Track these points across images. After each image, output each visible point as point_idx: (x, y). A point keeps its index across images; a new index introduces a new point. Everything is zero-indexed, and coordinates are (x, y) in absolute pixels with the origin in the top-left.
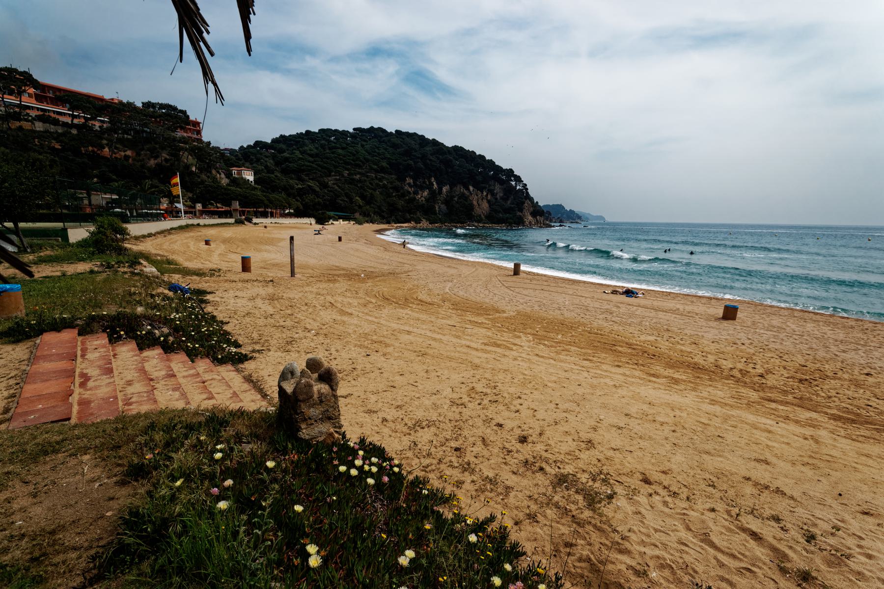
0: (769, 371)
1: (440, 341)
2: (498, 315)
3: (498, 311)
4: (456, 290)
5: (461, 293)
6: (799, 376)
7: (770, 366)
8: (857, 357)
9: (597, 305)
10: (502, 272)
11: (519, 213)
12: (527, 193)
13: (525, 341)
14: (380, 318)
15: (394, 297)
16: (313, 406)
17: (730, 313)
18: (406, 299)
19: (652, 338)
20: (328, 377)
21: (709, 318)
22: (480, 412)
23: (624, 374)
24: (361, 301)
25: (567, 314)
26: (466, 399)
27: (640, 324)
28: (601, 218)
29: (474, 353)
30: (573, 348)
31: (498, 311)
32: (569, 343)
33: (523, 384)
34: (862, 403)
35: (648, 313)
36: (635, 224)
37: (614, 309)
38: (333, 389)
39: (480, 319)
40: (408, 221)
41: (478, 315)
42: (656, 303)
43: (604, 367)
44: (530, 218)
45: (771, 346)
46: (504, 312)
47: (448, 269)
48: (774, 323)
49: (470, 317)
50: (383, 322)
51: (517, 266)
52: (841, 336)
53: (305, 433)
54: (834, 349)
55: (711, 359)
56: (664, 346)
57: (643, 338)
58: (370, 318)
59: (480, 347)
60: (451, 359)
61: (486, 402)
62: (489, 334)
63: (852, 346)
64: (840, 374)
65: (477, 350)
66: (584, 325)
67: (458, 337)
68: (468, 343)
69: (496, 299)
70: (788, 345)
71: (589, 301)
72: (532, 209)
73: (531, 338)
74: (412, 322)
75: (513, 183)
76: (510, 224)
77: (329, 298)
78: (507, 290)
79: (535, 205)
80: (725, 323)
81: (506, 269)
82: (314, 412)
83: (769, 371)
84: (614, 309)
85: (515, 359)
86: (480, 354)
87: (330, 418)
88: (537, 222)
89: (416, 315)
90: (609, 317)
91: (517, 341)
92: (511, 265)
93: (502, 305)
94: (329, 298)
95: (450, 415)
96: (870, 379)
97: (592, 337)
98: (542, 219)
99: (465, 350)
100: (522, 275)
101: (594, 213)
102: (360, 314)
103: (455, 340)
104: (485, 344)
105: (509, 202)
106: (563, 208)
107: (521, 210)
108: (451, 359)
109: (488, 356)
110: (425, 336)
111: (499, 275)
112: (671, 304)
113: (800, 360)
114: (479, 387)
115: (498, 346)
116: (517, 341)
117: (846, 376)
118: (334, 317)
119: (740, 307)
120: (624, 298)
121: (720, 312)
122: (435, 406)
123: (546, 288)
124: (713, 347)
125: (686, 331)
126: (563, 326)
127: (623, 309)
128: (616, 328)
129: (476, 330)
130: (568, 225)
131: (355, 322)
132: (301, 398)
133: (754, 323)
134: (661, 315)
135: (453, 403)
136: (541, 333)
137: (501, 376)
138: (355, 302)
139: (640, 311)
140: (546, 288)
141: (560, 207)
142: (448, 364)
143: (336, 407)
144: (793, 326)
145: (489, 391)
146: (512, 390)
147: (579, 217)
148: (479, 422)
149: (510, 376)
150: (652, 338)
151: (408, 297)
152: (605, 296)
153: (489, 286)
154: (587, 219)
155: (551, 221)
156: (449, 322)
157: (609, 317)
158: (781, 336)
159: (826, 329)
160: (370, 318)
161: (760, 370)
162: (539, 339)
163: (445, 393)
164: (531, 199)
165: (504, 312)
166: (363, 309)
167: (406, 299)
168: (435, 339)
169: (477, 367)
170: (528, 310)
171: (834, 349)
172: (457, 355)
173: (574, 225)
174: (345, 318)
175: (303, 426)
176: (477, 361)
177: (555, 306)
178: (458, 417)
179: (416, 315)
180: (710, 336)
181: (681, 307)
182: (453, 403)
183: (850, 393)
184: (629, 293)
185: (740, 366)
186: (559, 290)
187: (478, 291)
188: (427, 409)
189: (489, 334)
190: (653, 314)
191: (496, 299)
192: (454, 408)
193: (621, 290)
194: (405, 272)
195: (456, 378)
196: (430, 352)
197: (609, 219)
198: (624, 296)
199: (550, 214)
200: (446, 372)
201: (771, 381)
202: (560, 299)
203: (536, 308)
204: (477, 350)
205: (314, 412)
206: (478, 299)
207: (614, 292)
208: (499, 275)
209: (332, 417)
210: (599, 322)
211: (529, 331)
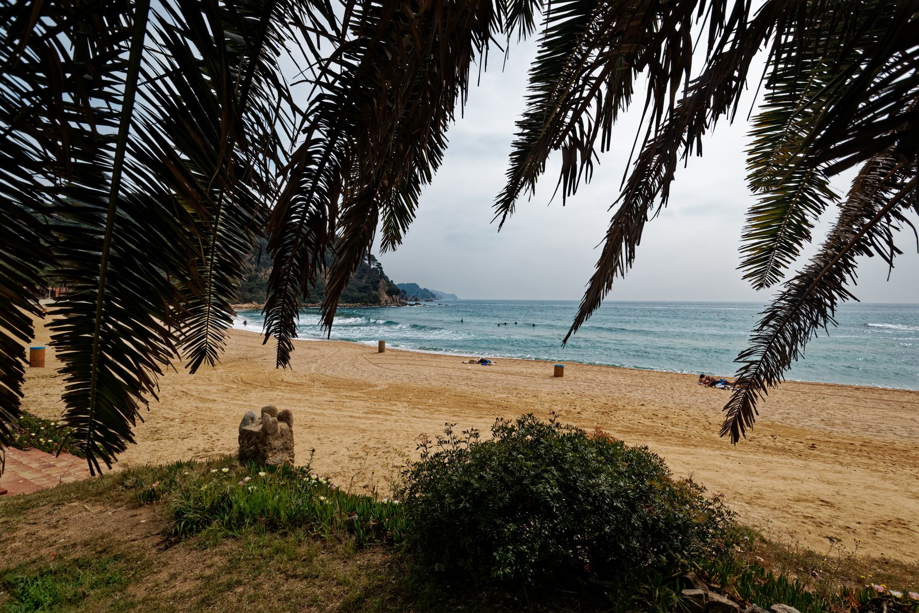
0: (584, 410)
1: (322, 414)
2: (371, 389)
3: (370, 386)
4: (323, 370)
5: (329, 373)
6: (603, 410)
7: (585, 406)
8: (637, 395)
9: (458, 373)
10: (367, 351)
11: (374, 292)
12: (382, 272)
13: (401, 407)
14: (250, 401)
15: (256, 381)
16: (276, 439)
17: (559, 372)
18: (271, 382)
19: (504, 396)
20: (286, 417)
21: (545, 377)
22: (378, 461)
23: (486, 422)
24: (219, 387)
25: (434, 383)
26: (362, 454)
27: (495, 385)
28: (454, 296)
29: (358, 420)
30: (443, 409)
31: (370, 386)
32: (440, 405)
33: (408, 438)
34: (635, 422)
35: (499, 377)
36: (527, 302)
37: (473, 376)
38: (290, 426)
39: (356, 394)
40: (250, 301)
41: (352, 390)
42: (505, 369)
43: (470, 419)
44: (386, 297)
45: (587, 393)
46: (376, 386)
47: (308, 351)
48: (589, 376)
49: (343, 393)
50: (254, 404)
51: (381, 344)
52: (629, 382)
53: (272, 460)
54: (624, 391)
55: (547, 405)
56: (513, 400)
57: (497, 396)
58: (239, 402)
59: (362, 416)
60: (338, 427)
61: (380, 453)
62: (368, 404)
63: (635, 388)
64: (627, 406)
65: (360, 418)
66: (449, 390)
67: (339, 410)
68: (350, 414)
69: (366, 375)
70: (597, 391)
71: (451, 371)
72: (387, 288)
73: (406, 404)
74: (287, 402)
75: (367, 262)
76: (366, 303)
77: (178, 387)
78: (374, 367)
79: (390, 284)
80: (556, 380)
81: (369, 347)
82: (277, 443)
83: (584, 410)
84: (473, 376)
85: (396, 421)
86: (364, 421)
87: (287, 449)
88: (393, 301)
89: (289, 396)
90: (469, 383)
91: (394, 408)
92: (375, 344)
93: (372, 380)
94: (178, 387)
95: (352, 466)
96: (643, 408)
97: (458, 399)
98: (398, 298)
99: (349, 419)
100: (387, 352)
101: (448, 292)
102: (225, 400)
103: (337, 413)
104: (367, 413)
105: (364, 281)
106: (418, 286)
107: (376, 289)
108: (338, 427)
109: (372, 421)
110: (306, 412)
111: (365, 353)
112: (517, 368)
113: (604, 400)
114: (371, 444)
115: (379, 413)
116: (394, 408)
117: (630, 408)
118: (195, 405)
119: (566, 367)
120: (480, 366)
121: (552, 372)
122: (336, 462)
123: (411, 362)
124: (548, 397)
125: (529, 388)
126: (431, 393)
127: (480, 375)
128: (476, 390)
129: (354, 403)
130: (423, 303)
131: (224, 407)
132: (270, 432)
133: (575, 378)
134: (510, 377)
135: (351, 458)
136: (414, 400)
137: (388, 434)
138: (213, 389)
139: (493, 376)
140: (411, 362)
141: (414, 286)
142: (337, 431)
143: (292, 440)
144: (601, 378)
145: (380, 446)
146: (400, 443)
147: (434, 296)
148: (379, 468)
149: (395, 434)
150: (504, 396)
151: (272, 380)
152: (464, 366)
153: (357, 364)
154: (441, 297)
155: (406, 299)
156: (325, 399)
157: (469, 383)
158: (593, 385)
159: (620, 378)
160: (239, 402)
161: (578, 410)
162: (413, 405)
163: (342, 453)
164: (386, 278)
165: (376, 386)
166: (226, 395)
167: (271, 382)
168: (316, 414)
169: (364, 431)
170: (399, 382)
171: (624, 391)
172: (343, 424)
173: (428, 304)
174: (210, 405)
175: (270, 455)
176: (362, 426)
177: (422, 377)
178: (359, 466)
179: (289, 396)
180: (546, 390)
181: (525, 370)
182: (351, 458)
183: (630, 417)
184: (483, 362)
185: (565, 408)
186: (424, 363)
187: (346, 369)
188: (329, 466)
189: (368, 404)
190: (504, 377)
191: (366, 375)
192: (354, 461)
193: (476, 360)
194: (260, 356)
195: (348, 441)
196: (316, 424)
197: (461, 297)
198: (480, 365)
199: (405, 293)
200: (337, 437)
201: (585, 415)
202: (426, 371)
203: (406, 380)
204: (360, 418)
205: (277, 443)
206: (348, 377)
207: (472, 362)
208: (365, 353)
209: (288, 448)
210: (462, 388)
211: (403, 399)
